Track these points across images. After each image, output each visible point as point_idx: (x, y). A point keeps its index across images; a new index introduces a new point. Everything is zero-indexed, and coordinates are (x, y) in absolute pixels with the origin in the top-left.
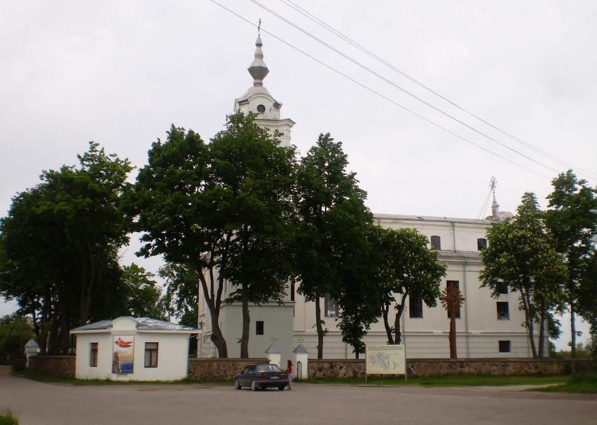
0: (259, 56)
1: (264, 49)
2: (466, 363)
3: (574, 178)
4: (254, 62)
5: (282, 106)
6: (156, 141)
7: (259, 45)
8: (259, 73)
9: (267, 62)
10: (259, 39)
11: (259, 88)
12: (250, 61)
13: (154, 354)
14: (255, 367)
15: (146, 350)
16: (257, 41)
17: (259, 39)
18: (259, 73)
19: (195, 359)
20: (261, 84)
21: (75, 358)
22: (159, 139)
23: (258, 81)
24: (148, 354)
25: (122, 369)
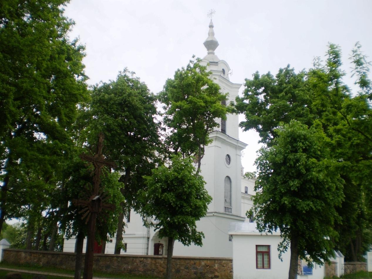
0: (212, 34)
1: (214, 29)
2: (115, 258)
3: (244, 128)
4: (208, 38)
5: (342, 65)
6: (358, 85)
7: (211, 26)
8: (211, 45)
9: (217, 38)
10: (211, 22)
11: (211, 55)
12: (205, 37)
13: (266, 257)
14: (154, 264)
15: (258, 253)
16: (210, 23)
17: (211, 22)
18: (211, 45)
19: (118, 255)
20: (214, 54)
21: (366, 264)
22: (356, 83)
23: (210, 51)
24: (260, 257)
25: (304, 271)
